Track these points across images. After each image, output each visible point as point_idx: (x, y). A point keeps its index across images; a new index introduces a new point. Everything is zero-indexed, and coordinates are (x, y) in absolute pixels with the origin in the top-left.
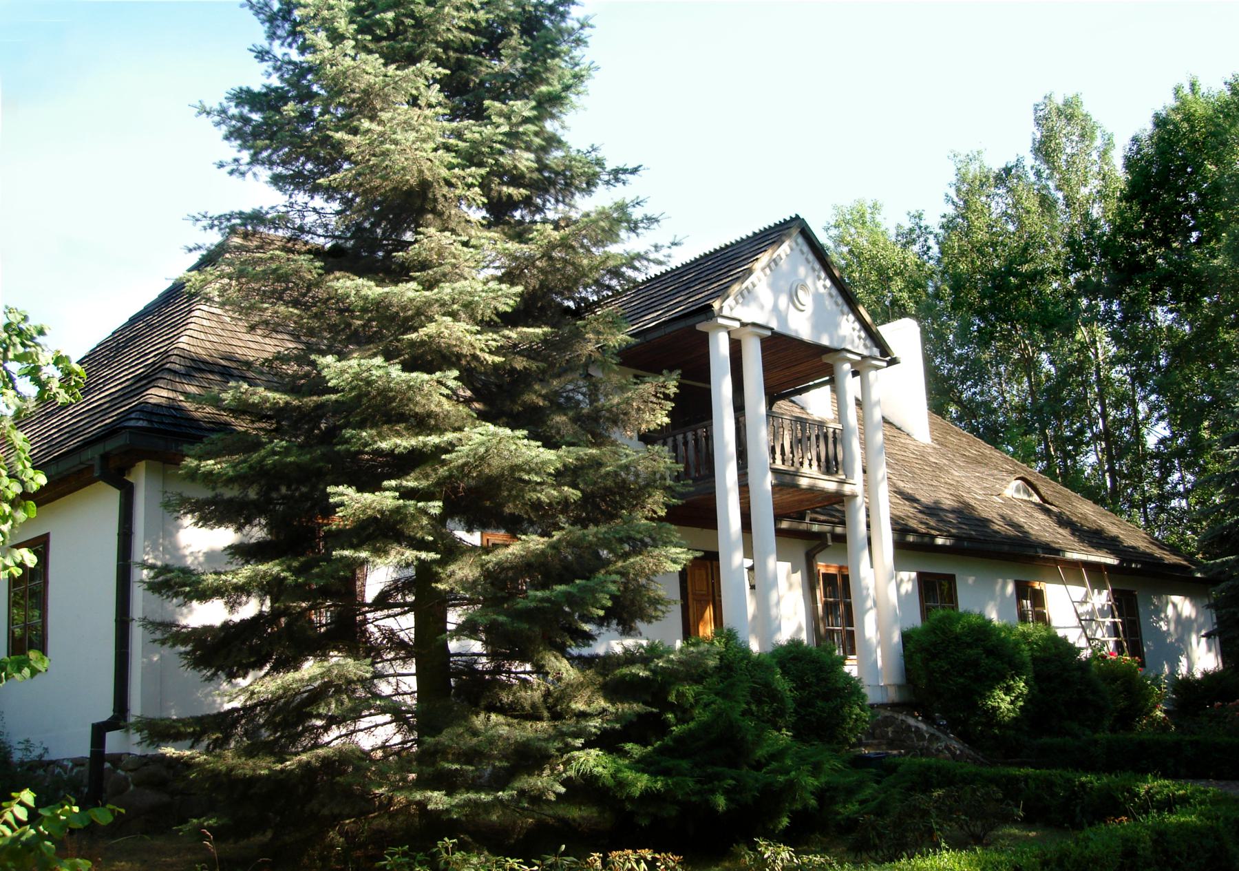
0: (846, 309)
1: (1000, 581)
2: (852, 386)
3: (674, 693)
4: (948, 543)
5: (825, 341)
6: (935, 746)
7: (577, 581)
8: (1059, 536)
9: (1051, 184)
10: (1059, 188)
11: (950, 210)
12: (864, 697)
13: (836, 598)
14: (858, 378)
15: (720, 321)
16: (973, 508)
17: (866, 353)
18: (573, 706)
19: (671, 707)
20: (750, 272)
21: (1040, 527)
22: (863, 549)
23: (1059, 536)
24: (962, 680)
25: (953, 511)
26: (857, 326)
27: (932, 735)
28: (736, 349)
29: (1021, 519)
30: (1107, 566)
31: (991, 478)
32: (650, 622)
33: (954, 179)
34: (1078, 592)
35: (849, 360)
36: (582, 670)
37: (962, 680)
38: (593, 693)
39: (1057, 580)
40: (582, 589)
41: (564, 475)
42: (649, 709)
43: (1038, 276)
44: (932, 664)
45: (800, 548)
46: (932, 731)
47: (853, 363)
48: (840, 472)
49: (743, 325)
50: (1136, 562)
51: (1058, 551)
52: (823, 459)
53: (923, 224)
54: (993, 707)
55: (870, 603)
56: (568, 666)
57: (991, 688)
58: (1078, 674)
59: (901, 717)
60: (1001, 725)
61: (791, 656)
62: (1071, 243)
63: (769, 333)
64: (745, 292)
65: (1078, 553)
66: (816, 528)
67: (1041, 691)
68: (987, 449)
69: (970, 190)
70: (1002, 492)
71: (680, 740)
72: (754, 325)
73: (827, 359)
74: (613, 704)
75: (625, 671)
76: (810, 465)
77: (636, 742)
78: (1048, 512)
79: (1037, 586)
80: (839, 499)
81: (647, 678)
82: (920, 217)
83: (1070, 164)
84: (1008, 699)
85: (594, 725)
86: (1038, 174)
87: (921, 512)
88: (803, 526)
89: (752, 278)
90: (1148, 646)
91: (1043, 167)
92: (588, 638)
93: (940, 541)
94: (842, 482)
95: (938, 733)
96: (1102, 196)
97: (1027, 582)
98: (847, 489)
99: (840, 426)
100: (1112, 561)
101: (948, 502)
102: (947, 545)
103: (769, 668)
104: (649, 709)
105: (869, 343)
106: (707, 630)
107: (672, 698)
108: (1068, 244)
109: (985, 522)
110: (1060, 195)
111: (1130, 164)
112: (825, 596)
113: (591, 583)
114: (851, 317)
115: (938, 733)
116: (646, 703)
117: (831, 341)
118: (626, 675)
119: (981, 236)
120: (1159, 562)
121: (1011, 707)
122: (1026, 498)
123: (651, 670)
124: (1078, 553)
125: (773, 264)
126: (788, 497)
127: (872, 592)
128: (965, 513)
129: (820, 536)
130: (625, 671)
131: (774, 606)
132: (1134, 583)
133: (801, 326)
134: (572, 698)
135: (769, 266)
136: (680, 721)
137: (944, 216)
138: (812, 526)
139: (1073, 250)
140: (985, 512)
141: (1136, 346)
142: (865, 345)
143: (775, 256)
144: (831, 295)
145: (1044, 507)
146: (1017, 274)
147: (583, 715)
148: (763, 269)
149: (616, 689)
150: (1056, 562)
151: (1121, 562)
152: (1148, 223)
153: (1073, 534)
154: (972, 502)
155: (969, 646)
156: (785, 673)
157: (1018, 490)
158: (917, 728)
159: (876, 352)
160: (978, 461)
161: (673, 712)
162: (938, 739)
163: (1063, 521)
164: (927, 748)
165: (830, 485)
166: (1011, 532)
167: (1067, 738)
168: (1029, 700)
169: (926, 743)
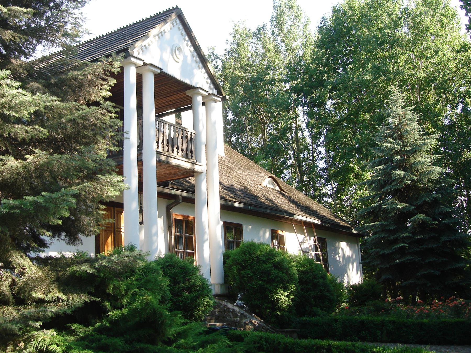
0: (201, 65)
1: (263, 229)
2: (202, 110)
3: (111, 287)
4: (241, 206)
5: (187, 81)
6: (244, 321)
7: (44, 194)
8: (292, 208)
9: (279, 38)
10: (282, 41)
11: (229, 47)
12: (210, 291)
13: (184, 232)
14: (205, 107)
15: (132, 59)
16: (250, 190)
17: (211, 92)
18: (34, 295)
19: (108, 297)
20: (147, 37)
21: (281, 202)
22: (204, 205)
23: (292, 208)
24: (260, 282)
25: (240, 190)
26: (206, 76)
27: (242, 314)
28: (139, 79)
29: (273, 198)
30: (315, 225)
31: (256, 176)
32: (88, 235)
33: (232, 31)
34: (301, 237)
35: (201, 94)
36: (40, 268)
37: (260, 282)
38: (50, 284)
39: (292, 231)
40: (46, 200)
41: (37, 117)
42: (93, 298)
43: (272, 82)
44: (242, 272)
45: (165, 203)
46: (242, 311)
47: (204, 97)
48: (194, 158)
49: (145, 64)
50: (328, 223)
51: (293, 215)
52: (185, 150)
53: (215, 53)
54: (277, 299)
55: (206, 237)
56: (30, 263)
57: (276, 288)
58: (321, 280)
59: (224, 303)
60: (280, 309)
61: (167, 265)
62: (289, 67)
63: (159, 71)
64: (144, 48)
65: (301, 217)
66: (173, 192)
67: (302, 289)
68: (251, 163)
69: (239, 39)
70: (262, 184)
71: (114, 323)
72: (151, 65)
73: (188, 93)
74: (66, 294)
75: (76, 268)
76: (178, 152)
77: (80, 323)
78: (284, 195)
79: (280, 232)
80: (192, 173)
81: (93, 274)
82: (213, 49)
83: (289, 31)
84: (286, 294)
85: (52, 309)
86: (273, 33)
87: (225, 189)
88: (166, 191)
89: (148, 41)
90: (331, 268)
91: (276, 30)
92: (43, 245)
93: (236, 205)
94: (193, 164)
95: (245, 313)
96: (305, 46)
97: (276, 230)
98: (197, 168)
99: (194, 132)
100: (318, 222)
101: (237, 186)
102: (242, 208)
103: (156, 271)
104: (93, 298)
105: (212, 86)
106: (109, 248)
107: (110, 290)
108: (288, 67)
109: (256, 197)
110: (283, 44)
111: (321, 30)
112: (175, 232)
113: (55, 195)
114: (203, 70)
115: (245, 313)
116: (90, 294)
117: (191, 82)
118: (75, 272)
119: (245, 61)
120: (337, 225)
121: (287, 299)
122: (272, 187)
123: (95, 268)
124: (301, 217)
125: (160, 35)
126: (163, 171)
127: (207, 230)
128: (245, 192)
129: (175, 197)
130: (76, 268)
131: (148, 236)
132: (327, 232)
133: (174, 71)
134: (33, 288)
135: (158, 35)
136: (115, 308)
137: (226, 50)
138: (176, 189)
139: (290, 71)
140: (254, 191)
141: (318, 121)
142: (210, 87)
143: (162, 30)
144: (193, 56)
145: (282, 192)
146: (262, 81)
147: (40, 302)
148: (154, 36)
149: (70, 283)
150: (292, 220)
151: (322, 223)
152: (328, 59)
153: (297, 207)
154: (249, 187)
155: (264, 262)
156: (165, 274)
157: (269, 183)
158: (233, 310)
159: (215, 92)
160: (250, 167)
161: (109, 301)
162: (245, 317)
163: (293, 201)
164: (239, 322)
165: (187, 166)
166: (268, 203)
167: (318, 317)
168: (296, 294)
169: (238, 319)
